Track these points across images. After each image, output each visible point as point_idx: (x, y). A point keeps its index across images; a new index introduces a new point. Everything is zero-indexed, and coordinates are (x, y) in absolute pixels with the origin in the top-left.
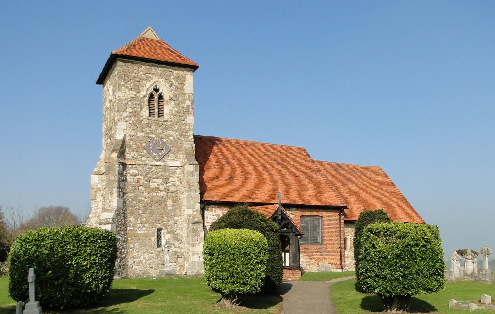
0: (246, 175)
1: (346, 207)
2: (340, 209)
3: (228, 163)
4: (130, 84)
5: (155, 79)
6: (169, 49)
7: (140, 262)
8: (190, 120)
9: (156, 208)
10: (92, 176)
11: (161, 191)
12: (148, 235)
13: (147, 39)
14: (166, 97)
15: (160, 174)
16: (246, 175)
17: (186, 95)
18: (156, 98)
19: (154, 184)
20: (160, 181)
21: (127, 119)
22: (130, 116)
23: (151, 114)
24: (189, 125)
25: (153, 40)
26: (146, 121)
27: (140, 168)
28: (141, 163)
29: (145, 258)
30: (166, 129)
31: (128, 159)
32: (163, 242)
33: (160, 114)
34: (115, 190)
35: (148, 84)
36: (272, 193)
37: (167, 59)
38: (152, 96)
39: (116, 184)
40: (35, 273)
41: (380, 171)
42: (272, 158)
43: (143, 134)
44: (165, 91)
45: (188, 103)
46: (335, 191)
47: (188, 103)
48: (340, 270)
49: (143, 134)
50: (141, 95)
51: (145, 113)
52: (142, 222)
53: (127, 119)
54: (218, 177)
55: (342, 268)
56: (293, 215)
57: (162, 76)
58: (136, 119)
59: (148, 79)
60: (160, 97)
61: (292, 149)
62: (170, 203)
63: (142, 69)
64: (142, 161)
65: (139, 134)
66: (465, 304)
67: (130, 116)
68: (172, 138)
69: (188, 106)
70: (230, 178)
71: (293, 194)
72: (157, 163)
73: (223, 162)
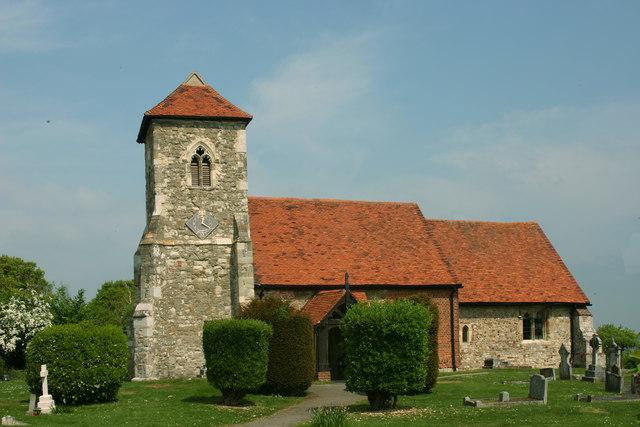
0: (323, 248)
2: (451, 290)
3: (302, 233)
4: (168, 148)
5: (198, 139)
6: (216, 99)
7: (182, 363)
9: (202, 297)
11: (208, 275)
12: (193, 330)
13: (191, 87)
15: (206, 255)
16: (323, 248)
17: (237, 155)
18: (201, 160)
19: (199, 267)
20: (205, 264)
21: (166, 190)
22: (169, 187)
24: (242, 192)
25: (198, 88)
27: (181, 249)
28: (183, 242)
29: (189, 356)
30: (212, 199)
31: (168, 239)
33: (208, 182)
36: (355, 271)
37: (213, 113)
38: (195, 160)
40: (208, 352)
42: (365, 222)
43: (184, 207)
44: (213, 153)
46: (448, 264)
48: (450, 370)
49: (184, 207)
52: (186, 314)
53: (166, 190)
54: (284, 254)
55: (454, 368)
57: (206, 135)
59: (189, 140)
60: (206, 160)
61: (398, 207)
63: (180, 132)
64: (183, 239)
65: (180, 208)
67: (169, 187)
68: (220, 210)
69: (240, 169)
70: (301, 253)
71: (386, 271)
72: (202, 242)
73: (295, 232)
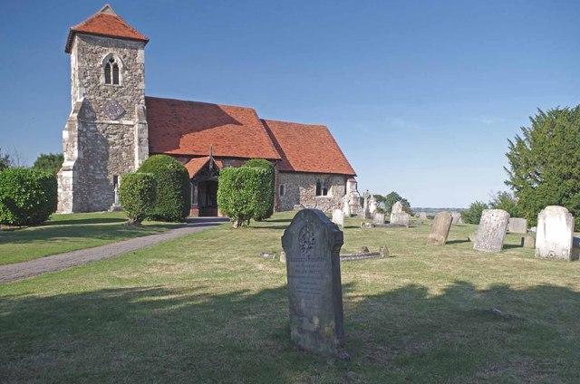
1: (355, 175)
3: (180, 122)
5: (110, 50)
8: (142, 85)
10: (64, 132)
14: (120, 66)
23: (108, 81)
26: (103, 87)
30: (123, 94)
32: (285, 192)
33: (116, 81)
34: (76, 143)
35: (104, 56)
39: (76, 139)
41: (325, 129)
45: (140, 71)
47: (140, 71)
50: (98, 65)
51: (102, 80)
56: (219, 163)
58: (94, 85)
60: (116, 67)
62: (124, 154)
66: (404, 277)
72: (113, 122)
